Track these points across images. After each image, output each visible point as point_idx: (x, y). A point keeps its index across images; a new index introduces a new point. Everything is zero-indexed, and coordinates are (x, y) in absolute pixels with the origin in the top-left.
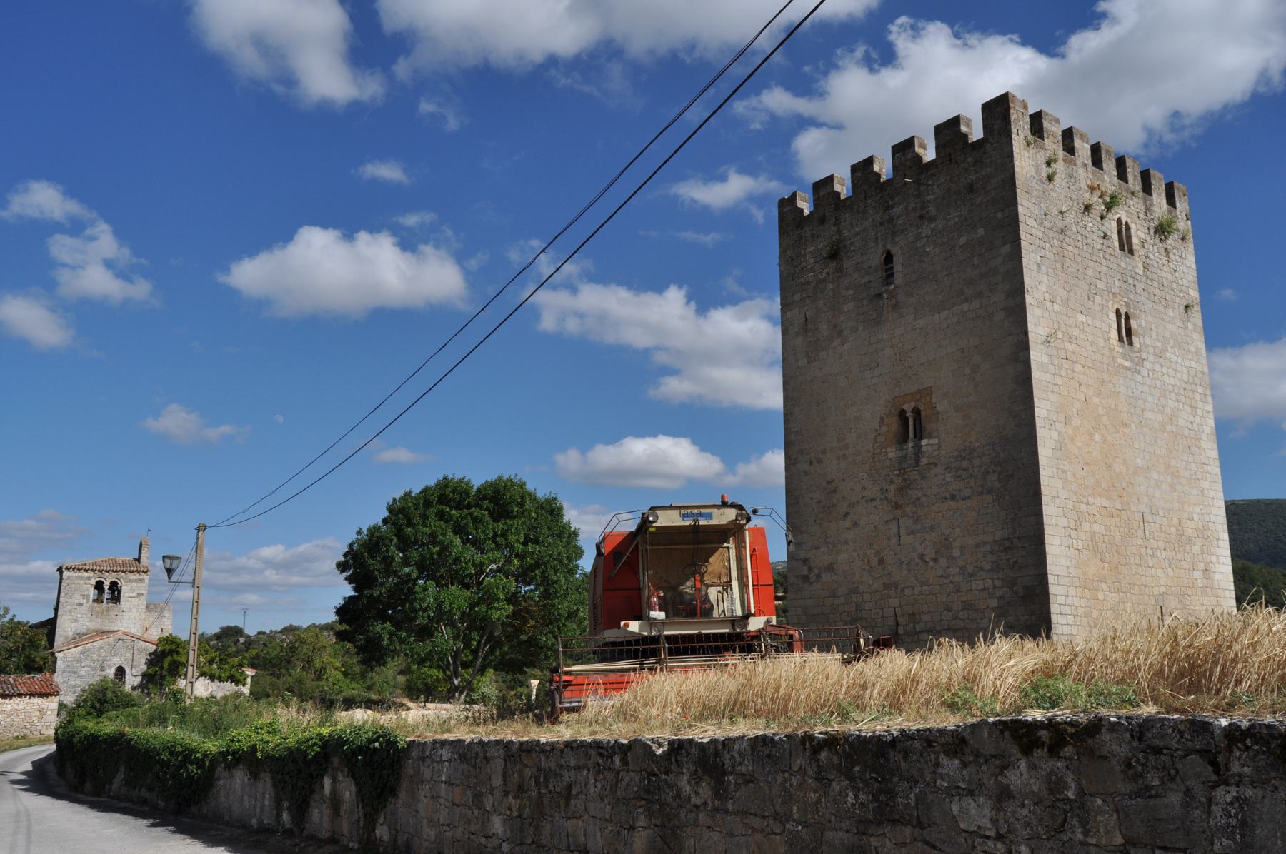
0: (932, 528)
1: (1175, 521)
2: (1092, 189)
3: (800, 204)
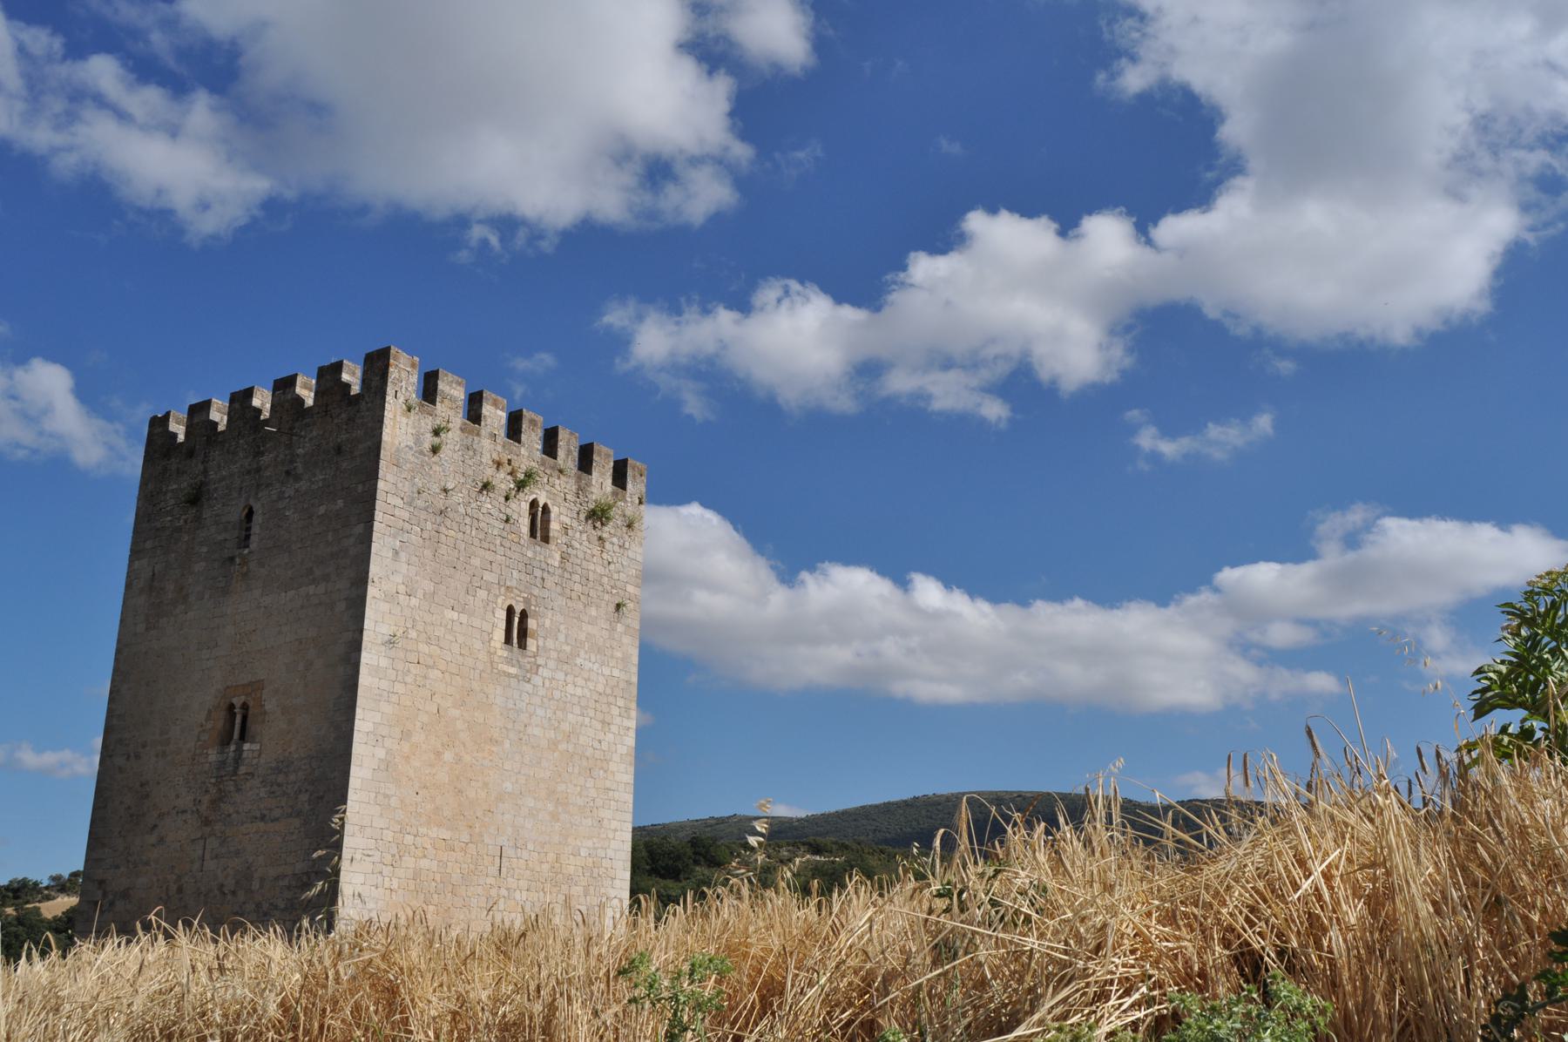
0: (237, 853)
1: (551, 857)
2: (499, 464)
3: (299, 390)
